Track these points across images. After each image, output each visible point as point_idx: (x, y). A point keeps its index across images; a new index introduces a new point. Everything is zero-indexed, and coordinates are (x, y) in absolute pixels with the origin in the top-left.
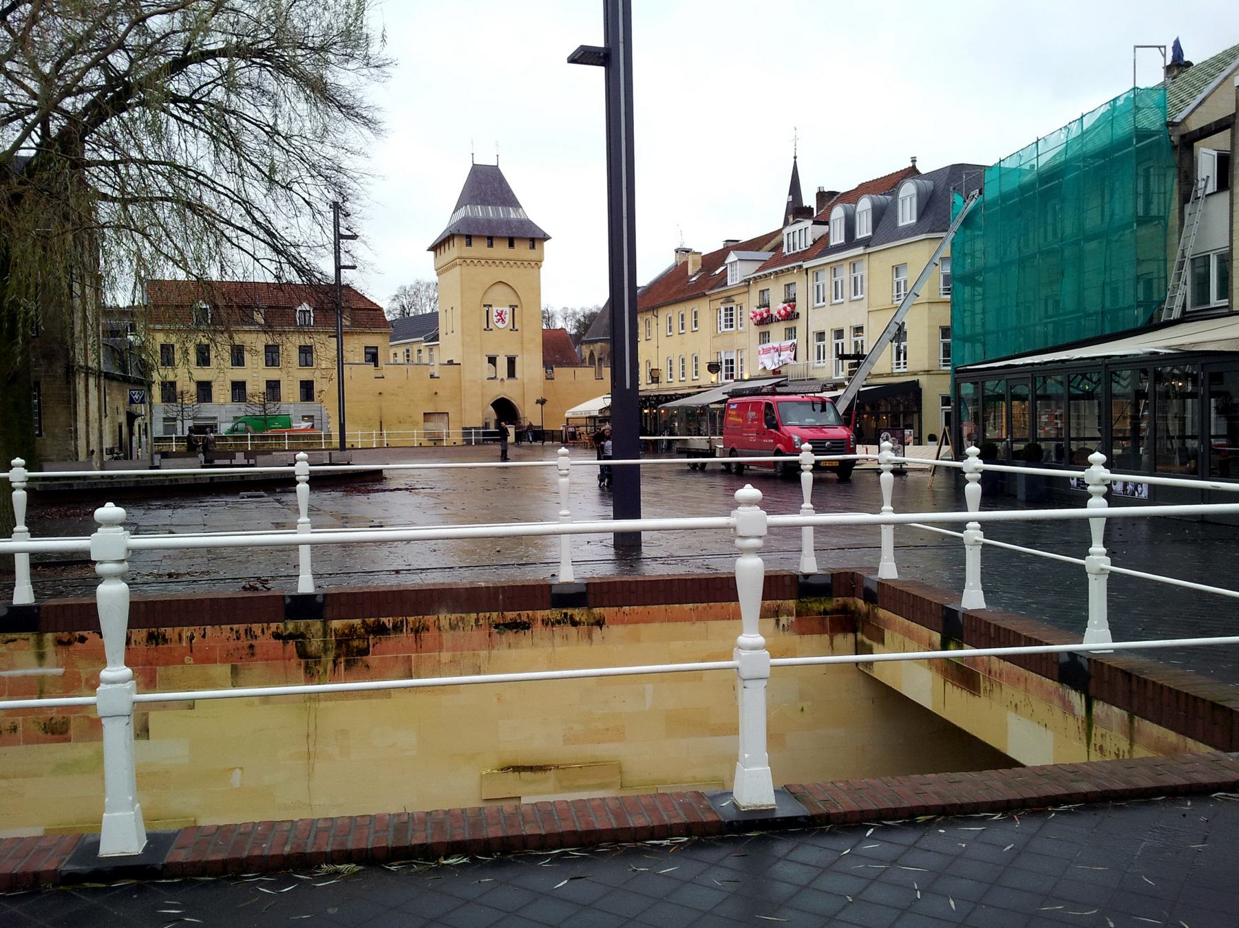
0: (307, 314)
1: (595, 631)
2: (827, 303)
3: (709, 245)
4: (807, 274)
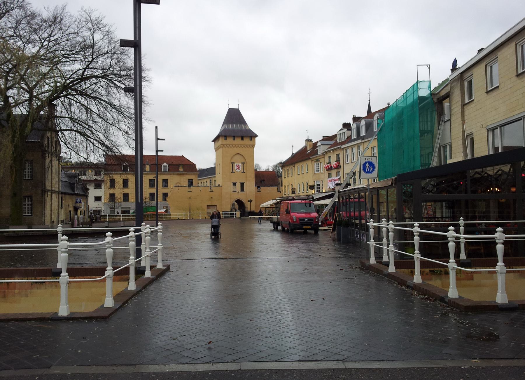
0: (166, 167)
4: (343, 150)
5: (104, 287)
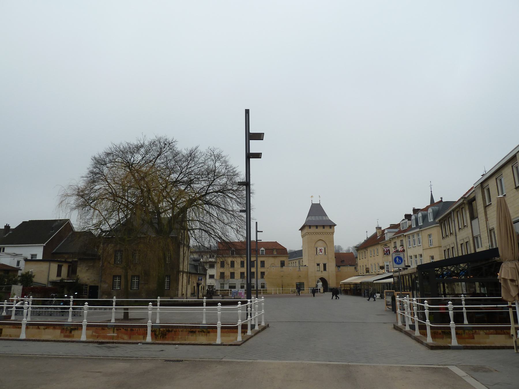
4: (405, 237)
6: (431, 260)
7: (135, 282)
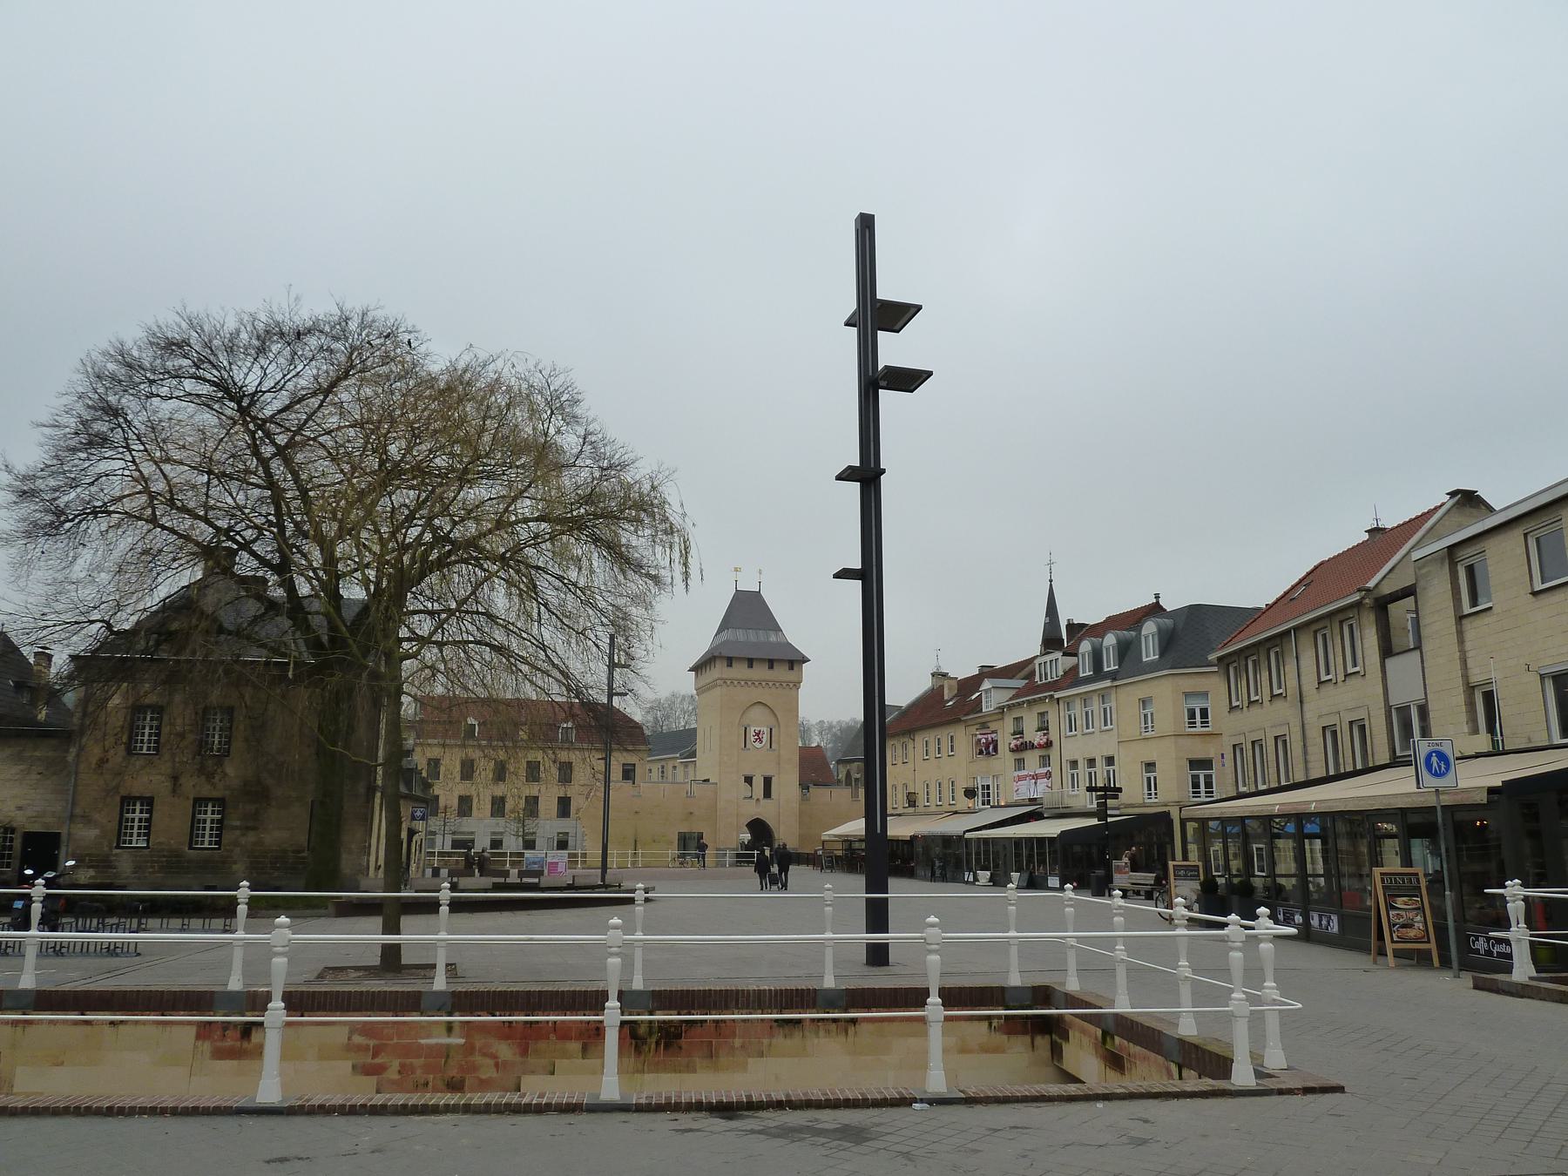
1: (849, 1027)
2: (1078, 733)
3: (964, 669)
5: (925, 1034)
6: (1144, 774)
7: (208, 822)
